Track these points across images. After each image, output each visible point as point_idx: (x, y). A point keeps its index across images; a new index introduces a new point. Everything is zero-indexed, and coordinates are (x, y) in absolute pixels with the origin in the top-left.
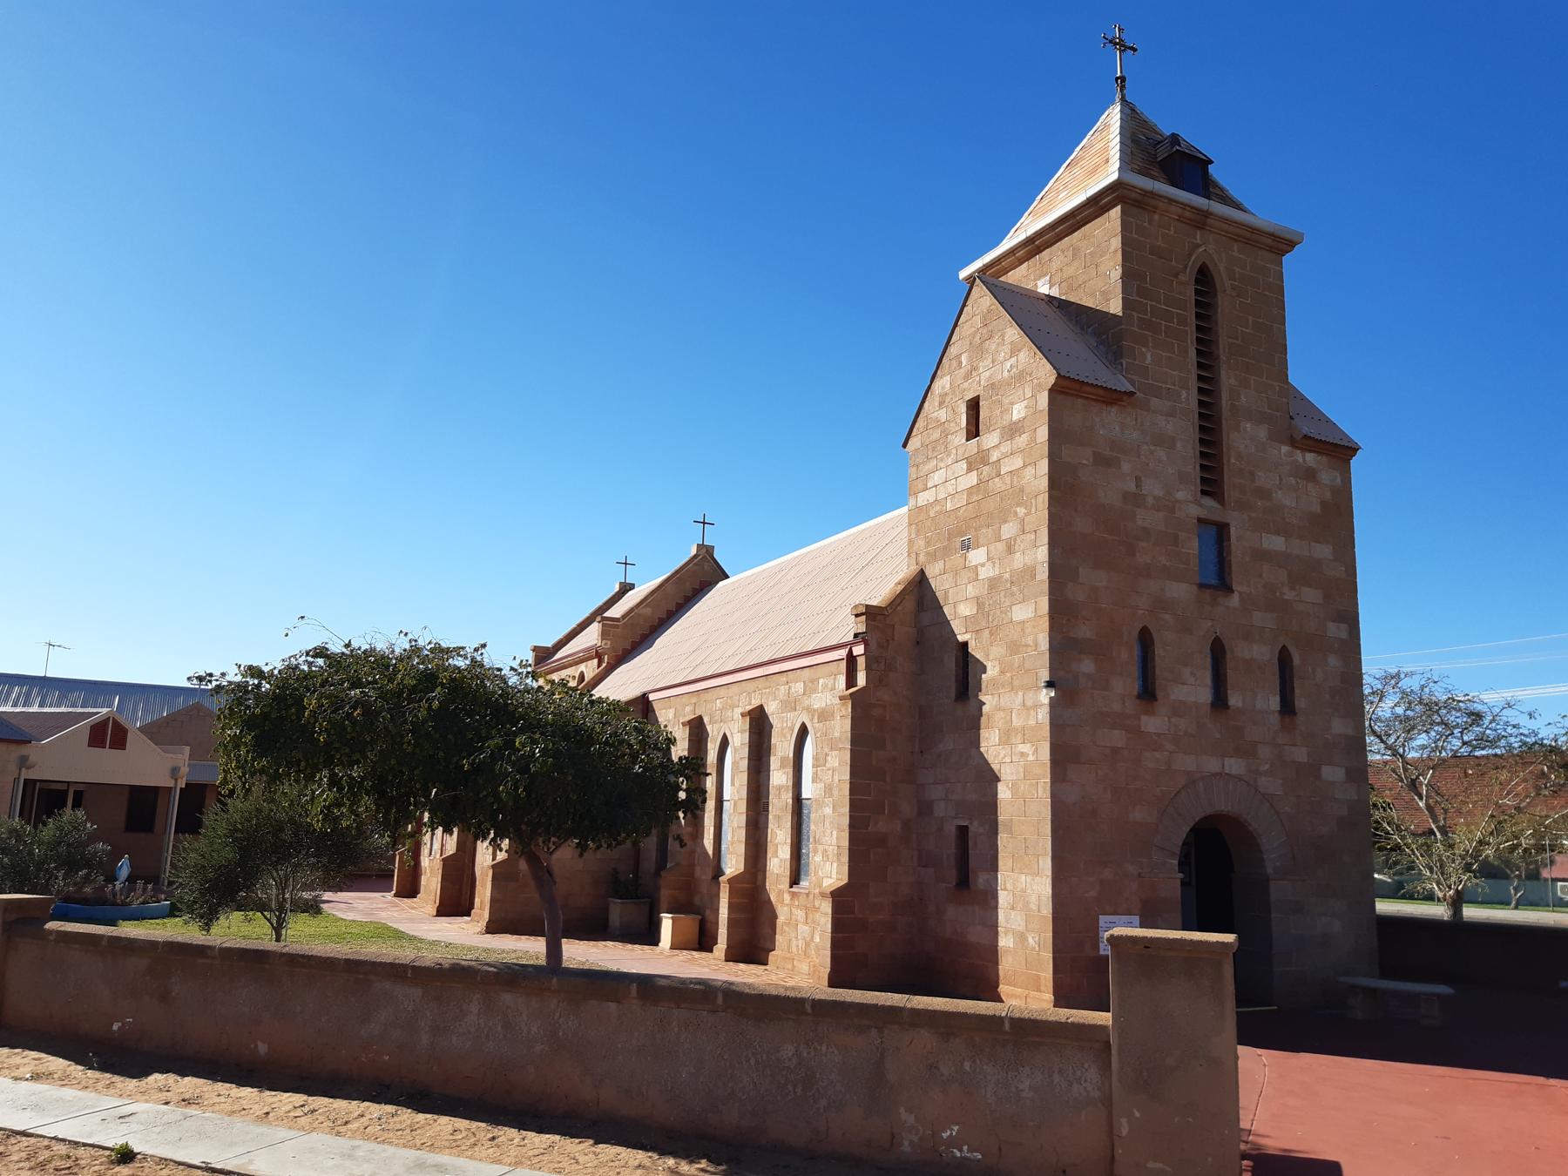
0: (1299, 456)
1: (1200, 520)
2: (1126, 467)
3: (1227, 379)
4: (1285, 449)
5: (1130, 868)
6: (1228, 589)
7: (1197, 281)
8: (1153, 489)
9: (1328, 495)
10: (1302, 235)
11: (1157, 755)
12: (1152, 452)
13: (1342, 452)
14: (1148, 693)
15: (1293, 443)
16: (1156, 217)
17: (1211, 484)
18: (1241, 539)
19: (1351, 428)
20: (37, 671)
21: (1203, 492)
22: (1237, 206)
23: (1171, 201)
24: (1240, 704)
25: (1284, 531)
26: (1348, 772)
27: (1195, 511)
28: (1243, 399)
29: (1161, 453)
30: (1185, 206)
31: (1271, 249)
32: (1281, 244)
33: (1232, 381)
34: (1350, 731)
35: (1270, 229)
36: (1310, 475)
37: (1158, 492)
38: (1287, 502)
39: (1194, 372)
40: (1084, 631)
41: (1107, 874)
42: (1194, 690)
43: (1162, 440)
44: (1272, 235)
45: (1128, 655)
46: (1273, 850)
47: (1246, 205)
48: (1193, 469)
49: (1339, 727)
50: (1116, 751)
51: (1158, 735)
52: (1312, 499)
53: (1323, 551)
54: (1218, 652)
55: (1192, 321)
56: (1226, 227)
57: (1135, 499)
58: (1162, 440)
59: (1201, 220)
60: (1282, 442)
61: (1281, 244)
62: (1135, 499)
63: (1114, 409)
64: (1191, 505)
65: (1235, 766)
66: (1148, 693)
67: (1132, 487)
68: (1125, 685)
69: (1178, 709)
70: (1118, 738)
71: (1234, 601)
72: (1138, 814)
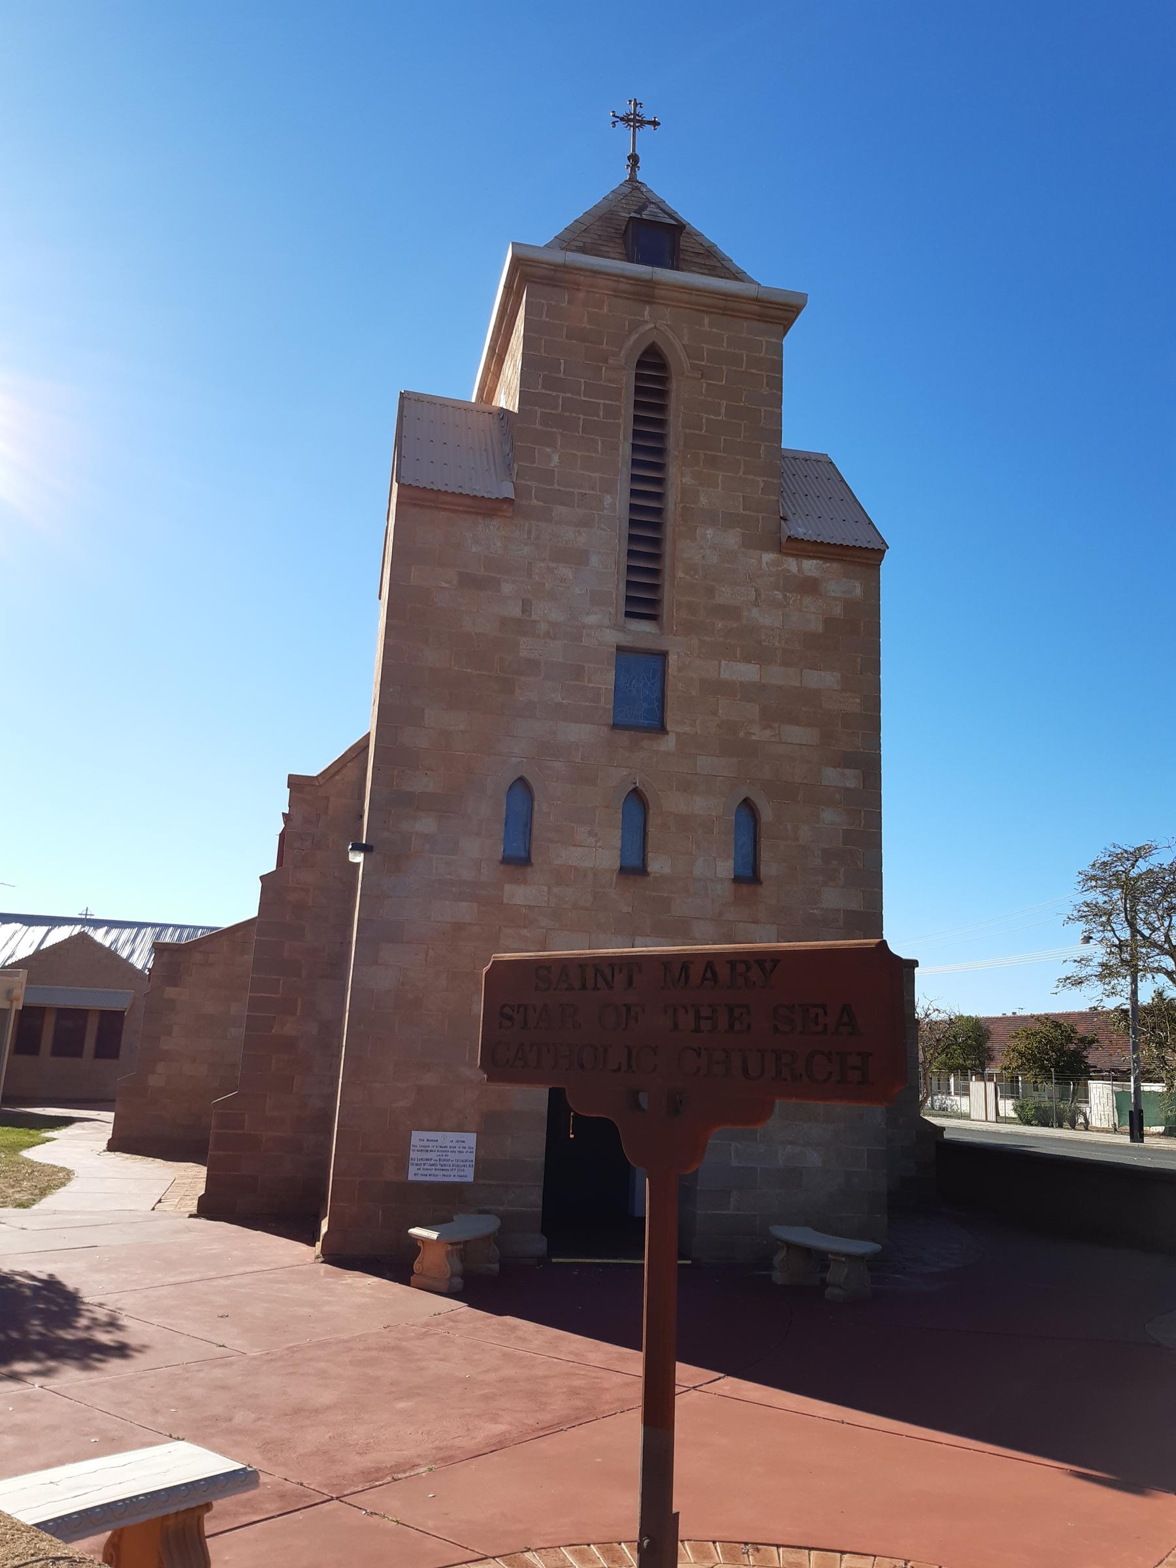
0: (792, 564)
1: (620, 649)
2: (507, 588)
3: (679, 477)
4: (768, 557)
6: (662, 729)
7: (640, 364)
9: (838, 611)
11: (524, 932)
13: (866, 557)
14: (518, 861)
16: (581, 295)
17: (643, 597)
18: (686, 664)
20: (670, 694)
21: (628, 614)
23: (595, 273)
24: (667, 870)
25: (759, 655)
27: (612, 638)
28: (703, 500)
29: (565, 571)
30: (617, 277)
31: (761, 318)
32: (780, 313)
33: (687, 480)
36: (810, 586)
37: (557, 616)
38: (767, 621)
39: (625, 471)
40: (424, 783)
42: (600, 852)
43: (579, 558)
44: (757, 300)
45: (487, 809)
48: (615, 587)
50: (458, 927)
51: (530, 907)
52: (809, 616)
53: (825, 680)
54: (637, 799)
55: (628, 411)
56: (686, 297)
58: (579, 558)
60: (766, 549)
61: (780, 313)
63: (495, 522)
64: (606, 629)
67: (515, 611)
68: (478, 848)
70: (465, 911)
71: (669, 743)
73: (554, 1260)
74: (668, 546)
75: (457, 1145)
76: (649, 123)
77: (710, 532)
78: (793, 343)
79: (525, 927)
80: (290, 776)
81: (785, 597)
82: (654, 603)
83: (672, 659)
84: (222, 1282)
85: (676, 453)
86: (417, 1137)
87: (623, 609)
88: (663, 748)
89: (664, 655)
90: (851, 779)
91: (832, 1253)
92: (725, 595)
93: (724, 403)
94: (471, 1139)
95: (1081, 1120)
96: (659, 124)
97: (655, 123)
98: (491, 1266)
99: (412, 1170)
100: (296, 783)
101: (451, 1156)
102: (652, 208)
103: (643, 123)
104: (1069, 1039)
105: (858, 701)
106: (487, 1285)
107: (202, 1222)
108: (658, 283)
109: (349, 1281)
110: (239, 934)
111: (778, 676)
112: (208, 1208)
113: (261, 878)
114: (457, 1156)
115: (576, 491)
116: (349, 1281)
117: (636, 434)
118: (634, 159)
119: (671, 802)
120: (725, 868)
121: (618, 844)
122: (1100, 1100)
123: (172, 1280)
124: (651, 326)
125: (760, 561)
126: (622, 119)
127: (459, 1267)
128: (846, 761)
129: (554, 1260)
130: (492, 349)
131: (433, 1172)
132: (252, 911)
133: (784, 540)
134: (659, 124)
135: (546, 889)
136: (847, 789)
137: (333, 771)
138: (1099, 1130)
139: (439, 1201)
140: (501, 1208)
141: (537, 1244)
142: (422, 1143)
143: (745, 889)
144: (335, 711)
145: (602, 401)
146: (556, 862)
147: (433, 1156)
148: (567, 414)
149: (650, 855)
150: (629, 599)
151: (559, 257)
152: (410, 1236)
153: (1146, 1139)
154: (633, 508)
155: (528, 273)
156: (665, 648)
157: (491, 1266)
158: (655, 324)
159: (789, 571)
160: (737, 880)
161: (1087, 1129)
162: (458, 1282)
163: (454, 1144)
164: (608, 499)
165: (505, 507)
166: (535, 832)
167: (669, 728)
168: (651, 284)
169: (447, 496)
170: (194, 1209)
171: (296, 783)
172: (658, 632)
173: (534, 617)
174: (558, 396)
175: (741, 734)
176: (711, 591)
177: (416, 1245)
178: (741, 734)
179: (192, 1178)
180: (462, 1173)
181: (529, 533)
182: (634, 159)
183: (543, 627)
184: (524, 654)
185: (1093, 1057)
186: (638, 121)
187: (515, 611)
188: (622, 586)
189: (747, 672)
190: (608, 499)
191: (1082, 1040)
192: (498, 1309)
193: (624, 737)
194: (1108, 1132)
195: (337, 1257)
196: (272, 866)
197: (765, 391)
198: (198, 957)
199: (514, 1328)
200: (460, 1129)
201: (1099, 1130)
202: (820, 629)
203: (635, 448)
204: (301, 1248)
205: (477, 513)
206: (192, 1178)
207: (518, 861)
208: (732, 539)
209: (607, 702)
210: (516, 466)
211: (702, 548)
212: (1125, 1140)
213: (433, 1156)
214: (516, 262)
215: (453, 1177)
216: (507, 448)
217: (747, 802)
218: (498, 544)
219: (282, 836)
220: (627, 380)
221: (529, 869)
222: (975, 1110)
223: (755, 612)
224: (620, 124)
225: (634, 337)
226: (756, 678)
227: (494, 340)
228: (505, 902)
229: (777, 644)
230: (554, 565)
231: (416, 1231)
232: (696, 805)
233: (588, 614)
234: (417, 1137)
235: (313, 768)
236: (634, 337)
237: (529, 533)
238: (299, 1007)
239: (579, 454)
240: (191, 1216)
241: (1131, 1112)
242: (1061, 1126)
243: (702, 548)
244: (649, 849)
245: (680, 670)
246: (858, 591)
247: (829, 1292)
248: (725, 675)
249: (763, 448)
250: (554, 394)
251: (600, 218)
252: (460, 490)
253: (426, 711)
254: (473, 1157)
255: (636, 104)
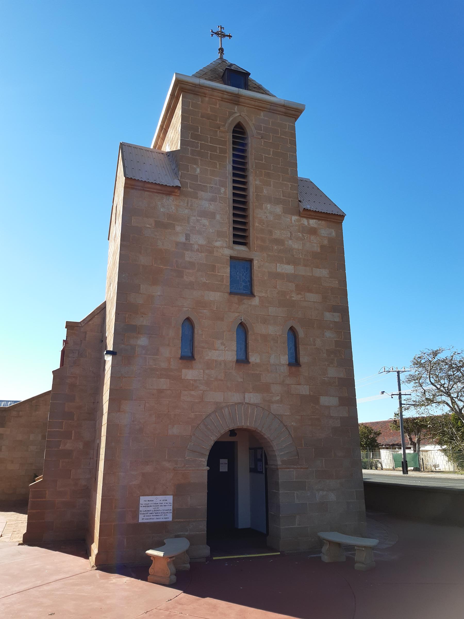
0: (305, 221)
1: (231, 258)
2: (178, 229)
3: (254, 181)
4: (294, 218)
5: (167, 465)
6: (252, 294)
7: (234, 131)
8: (198, 240)
9: (326, 242)
10: (304, 106)
11: (193, 393)
12: (198, 221)
13: (336, 218)
15: (300, 214)
16: (207, 99)
17: (241, 235)
19: (343, 206)
20: (255, 278)
21: (235, 243)
22: (265, 92)
23: (213, 89)
24: (258, 361)
25: (293, 261)
26: (341, 399)
27: (228, 252)
28: (265, 191)
29: (205, 221)
30: (223, 92)
31: (286, 114)
32: (293, 112)
33: (257, 182)
34: (342, 375)
35: (282, 103)
36: (313, 231)
37: (202, 241)
39: (230, 178)
41: (148, 469)
42: (226, 352)
43: (211, 215)
44: (284, 106)
45: (173, 333)
46: (281, 449)
47: (265, 86)
48: (228, 229)
49: (333, 372)
50: (160, 391)
51: (195, 381)
52: (314, 245)
53: (322, 273)
54: (243, 328)
55: (230, 152)
56: (253, 103)
57: (186, 246)
58: (211, 215)
59: (236, 100)
60: (293, 214)
61: (293, 112)
62: (186, 246)
63: (172, 198)
64: (225, 249)
65: (253, 398)
66: (188, 357)
68: (170, 352)
69: (209, 365)
71: (256, 301)
72: (175, 430)
73: (214, 558)
74: (251, 212)
75: (163, 502)
76: (227, 36)
77: (269, 206)
78: (299, 124)
79: (193, 390)
80: (67, 322)
81: (303, 236)
82: (244, 237)
83: (255, 263)
84: (46, 588)
85: (252, 170)
86: (143, 500)
87: (232, 239)
88: (253, 303)
89: (251, 261)
90: (336, 317)
91: (358, 546)
92: (277, 234)
93: (272, 150)
94: (170, 499)
95: (379, 465)
96: (231, 37)
97: (230, 36)
98: (185, 565)
99: (141, 517)
100: (70, 326)
101: (160, 508)
102: (234, 66)
103: (224, 36)
104: (370, 433)
105: (337, 282)
106: (191, 578)
107: (26, 547)
108: (241, 96)
109: (114, 581)
110: (34, 402)
111: (302, 271)
112: (30, 539)
113: (53, 372)
114: (163, 508)
115: (208, 185)
116: (114, 581)
117: (234, 162)
118: (221, 50)
119: (258, 329)
120: (284, 359)
121: (235, 349)
122: (386, 457)
123: (17, 589)
124: (239, 114)
125: (291, 220)
126: (216, 33)
127: (174, 570)
128: (334, 309)
129: (214, 558)
130: (162, 127)
131: (152, 517)
132: (49, 388)
133: (301, 210)
134: (231, 37)
135: (202, 371)
136: (335, 322)
137: (88, 319)
138: (387, 470)
139: (157, 533)
140: (186, 533)
141: (205, 550)
142: (146, 503)
143: (294, 369)
144: (96, 286)
145: (218, 146)
146: (206, 358)
147: (151, 509)
148: (203, 151)
149: (250, 354)
150: (234, 235)
151: (197, 81)
152: (149, 556)
153: (409, 472)
154: (234, 194)
155: (182, 87)
156: (252, 258)
157: (185, 565)
158: (239, 114)
159: (304, 224)
160: (290, 365)
161: (382, 469)
162: (174, 578)
163: (161, 502)
164: (223, 190)
165: (176, 190)
166: (196, 343)
167: (255, 294)
168: (238, 96)
169: (148, 188)
170: (21, 540)
171: (70, 326)
172: (248, 250)
173: (191, 242)
174: (198, 143)
175: (288, 297)
176: (271, 232)
177: (149, 560)
178: (288, 297)
179: (18, 522)
180: (166, 517)
181: (188, 203)
182: (221, 50)
183: (196, 247)
184: (187, 259)
185: (380, 440)
186: (222, 35)
187: (182, 239)
188: (231, 229)
189: (288, 269)
190: (223, 190)
191: (375, 433)
192: (202, 594)
193: (235, 299)
194: (391, 470)
195: (104, 565)
196: (58, 366)
197: (289, 145)
198: (14, 413)
199: (215, 607)
200: (164, 494)
201: (387, 470)
202: (319, 250)
203: (234, 168)
204: (81, 560)
205: (163, 193)
206: (18, 522)
207: (188, 357)
208: (278, 209)
209: (227, 281)
210: (180, 173)
211: (265, 213)
212: (401, 473)
213: (151, 509)
214: (178, 82)
215: (162, 519)
216: (174, 167)
217: (292, 329)
218: (173, 208)
219: (63, 352)
220: (229, 137)
221: (194, 362)
222: (385, 466)
223: (290, 242)
224: (215, 35)
225: (231, 119)
226: (293, 272)
227: (163, 122)
228: (183, 378)
229: (301, 257)
230: (200, 218)
231: (150, 552)
232: (269, 330)
233: (216, 241)
234: (143, 500)
235: (78, 318)
236: (231, 119)
237: (188, 203)
238: (73, 435)
239: (209, 169)
240: (19, 544)
241: (402, 462)
242: (371, 469)
243: (265, 213)
244: (250, 351)
245: (259, 267)
246: (334, 234)
247: (357, 566)
248: (279, 270)
249: (289, 170)
250: (197, 141)
251: (211, 70)
252: (155, 182)
253: (141, 285)
254: (171, 508)
255: (221, 28)
